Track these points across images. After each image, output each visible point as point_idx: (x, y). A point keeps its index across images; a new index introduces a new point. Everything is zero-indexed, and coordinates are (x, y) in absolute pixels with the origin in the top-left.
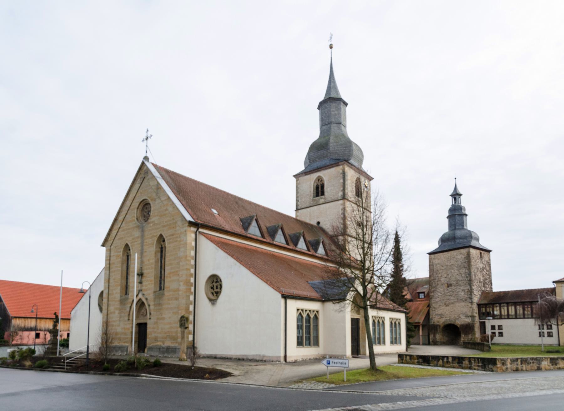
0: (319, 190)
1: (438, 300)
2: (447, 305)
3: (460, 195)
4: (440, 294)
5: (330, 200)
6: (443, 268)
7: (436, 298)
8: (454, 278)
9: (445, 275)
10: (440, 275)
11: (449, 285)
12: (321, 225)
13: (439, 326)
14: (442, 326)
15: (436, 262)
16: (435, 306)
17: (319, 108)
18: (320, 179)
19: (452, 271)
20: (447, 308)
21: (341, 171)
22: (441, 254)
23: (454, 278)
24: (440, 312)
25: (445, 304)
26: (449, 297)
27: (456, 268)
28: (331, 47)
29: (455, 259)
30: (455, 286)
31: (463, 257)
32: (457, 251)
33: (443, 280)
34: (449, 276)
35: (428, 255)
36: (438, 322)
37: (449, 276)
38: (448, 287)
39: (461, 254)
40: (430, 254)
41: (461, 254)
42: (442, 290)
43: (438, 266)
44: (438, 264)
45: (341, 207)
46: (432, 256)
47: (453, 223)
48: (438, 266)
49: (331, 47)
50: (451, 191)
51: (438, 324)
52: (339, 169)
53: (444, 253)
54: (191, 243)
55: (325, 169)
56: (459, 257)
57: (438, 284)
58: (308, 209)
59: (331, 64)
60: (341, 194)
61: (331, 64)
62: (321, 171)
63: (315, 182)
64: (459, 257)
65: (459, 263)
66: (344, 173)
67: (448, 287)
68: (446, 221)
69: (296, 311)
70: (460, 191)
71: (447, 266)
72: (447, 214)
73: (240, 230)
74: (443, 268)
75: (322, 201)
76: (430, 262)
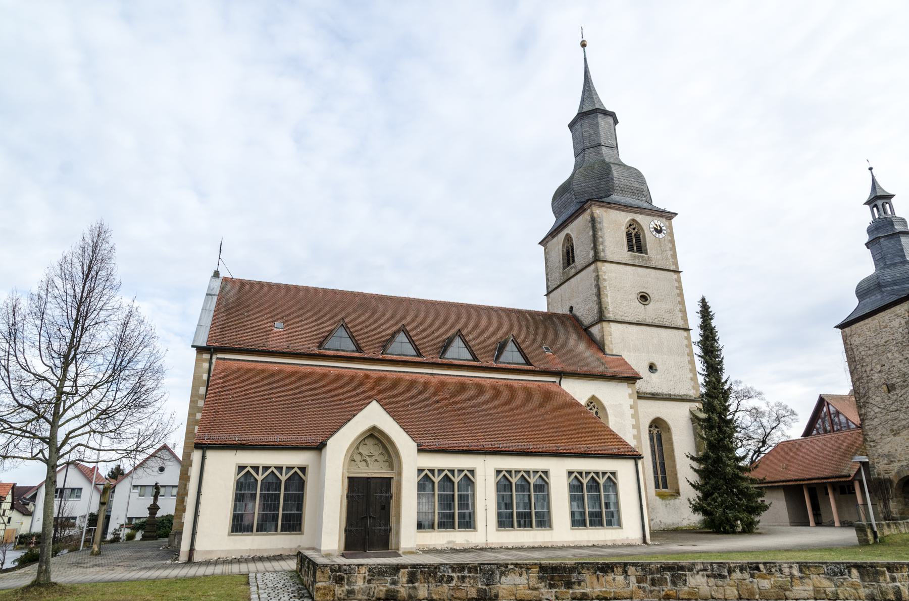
0: (569, 257)
1: (876, 422)
2: (896, 433)
3: (890, 197)
4: (877, 410)
5: (580, 268)
6: (871, 352)
7: (872, 419)
8: (895, 369)
9: (879, 367)
10: (868, 369)
11: (891, 388)
12: (575, 312)
13: (890, 481)
14: (896, 481)
15: (856, 340)
16: (874, 438)
17: (571, 126)
18: (568, 238)
19: (889, 355)
20: (897, 438)
21: (589, 218)
22: (862, 323)
23: (895, 369)
24: (886, 449)
25: (892, 431)
26: (896, 414)
27: (894, 349)
28: (583, 45)
29: (888, 329)
30: (902, 387)
31: (903, 322)
32: (888, 311)
33: (876, 377)
34: (886, 368)
35: (839, 330)
36: (887, 472)
37: (886, 368)
38: (889, 391)
39: (898, 316)
40: (842, 326)
41: (898, 316)
42: (878, 399)
43: (861, 349)
44: (861, 345)
45: (594, 275)
46: (847, 330)
47: (878, 256)
48: (861, 349)
49: (583, 45)
50: (867, 194)
51: (887, 476)
52: (585, 218)
53: (866, 321)
54: (202, 376)
55: (571, 222)
56: (896, 323)
57: (869, 388)
58: (559, 290)
59: (585, 59)
60: (592, 253)
61: (585, 59)
62: (567, 225)
63: (563, 245)
64: (896, 323)
65: (898, 336)
66: (593, 220)
67: (889, 391)
68: (867, 255)
69: (565, 475)
70: (887, 187)
71: (877, 346)
72: (866, 238)
73: (315, 350)
74: (871, 352)
75: (573, 271)
76: (845, 343)
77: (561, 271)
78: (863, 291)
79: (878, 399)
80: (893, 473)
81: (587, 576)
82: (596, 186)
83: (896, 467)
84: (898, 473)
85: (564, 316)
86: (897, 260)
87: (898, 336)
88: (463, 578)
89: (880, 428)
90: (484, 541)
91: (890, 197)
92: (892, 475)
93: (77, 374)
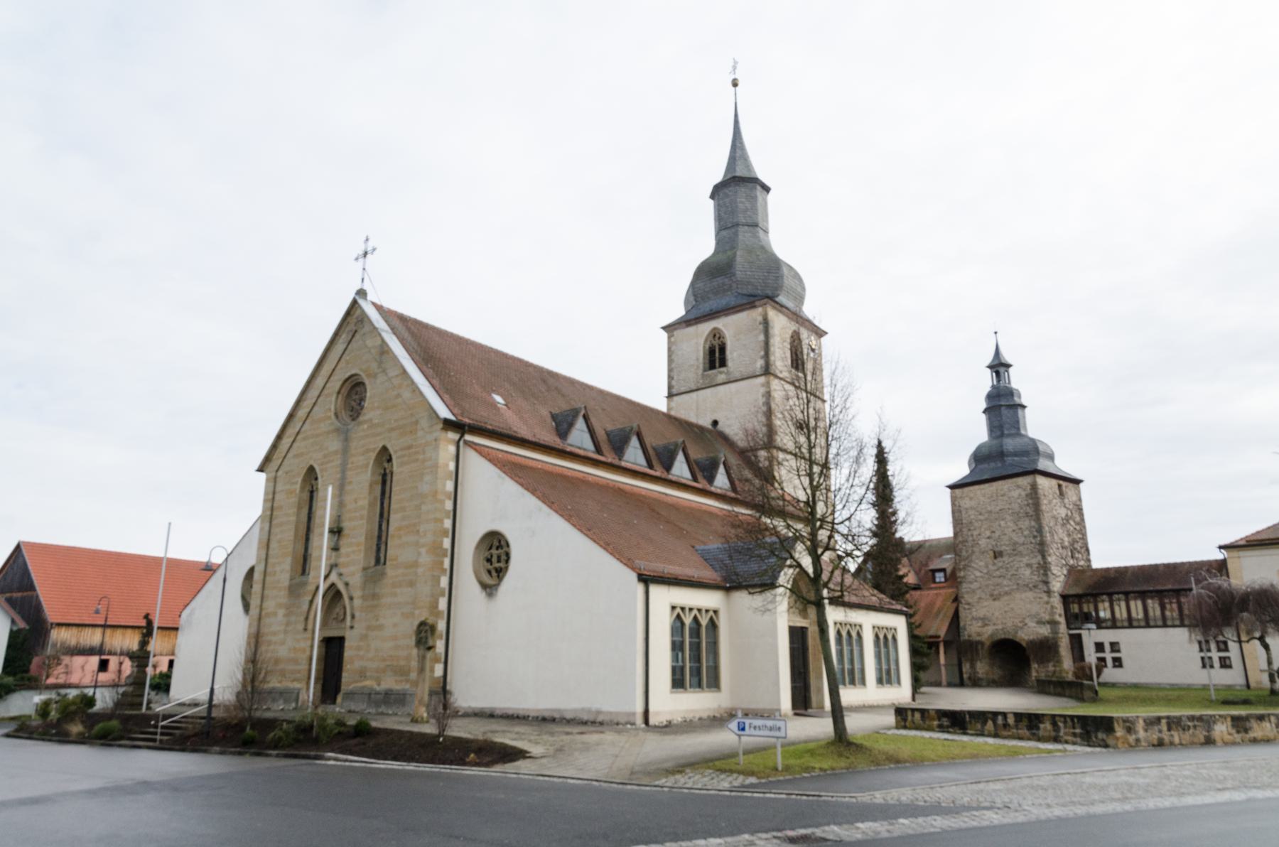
0: (716, 356)
1: (975, 586)
4: (978, 574)
8: (1006, 538)
9: (988, 533)
10: (975, 533)
11: (997, 555)
12: (721, 427)
13: (982, 643)
14: (988, 643)
15: (966, 503)
19: (1002, 523)
20: (997, 603)
21: (760, 319)
23: (1006, 538)
25: (992, 595)
26: (1000, 580)
27: (1009, 518)
30: (1010, 555)
31: (1023, 494)
32: (1010, 481)
33: (983, 542)
35: (949, 490)
36: (979, 634)
38: (995, 557)
39: (1019, 487)
40: (952, 487)
41: (1019, 487)
42: (982, 564)
44: (972, 508)
45: (762, 390)
46: (958, 491)
47: (996, 424)
48: (971, 512)
50: (989, 358)
51: (978, 638)
53: (982, 486)
55: (726, 315)
56: (1015, 493)
58: (694, 395)
59: (736, 115)
61: (736, 115)
64: (1015, 493)
65: (1016, 506)
67: (995, 557)
68: (982, 420)
70: (1007, 357)
71: (990, 512)
72: (984, 405)
75: (721, 378)
76: (953, 504)
77: (700, 372)
78: (979, 458)
79: (982, 564)
80: (986, 636)
81: (1254, 724)
82: (738, 283)
83: (989, 630)
84: (992, 636)
85: (701, 429)
86: (1013, 431)
87: (1016, 506)
88: (1195, 727)
89: (979, 592)
90: (203, 695)
91: (1008, 366)
92: (984, 638)
93: (793, 384)
